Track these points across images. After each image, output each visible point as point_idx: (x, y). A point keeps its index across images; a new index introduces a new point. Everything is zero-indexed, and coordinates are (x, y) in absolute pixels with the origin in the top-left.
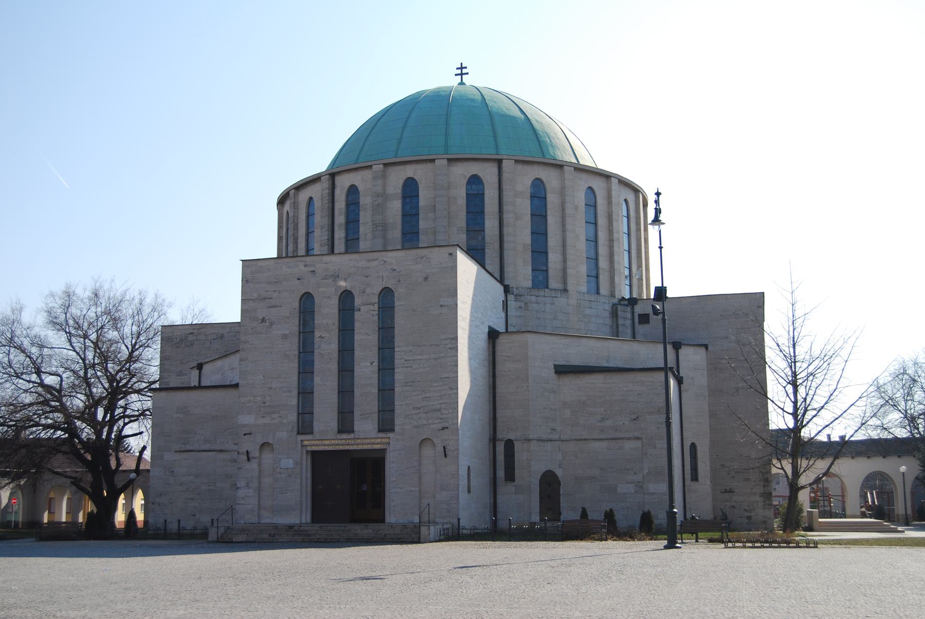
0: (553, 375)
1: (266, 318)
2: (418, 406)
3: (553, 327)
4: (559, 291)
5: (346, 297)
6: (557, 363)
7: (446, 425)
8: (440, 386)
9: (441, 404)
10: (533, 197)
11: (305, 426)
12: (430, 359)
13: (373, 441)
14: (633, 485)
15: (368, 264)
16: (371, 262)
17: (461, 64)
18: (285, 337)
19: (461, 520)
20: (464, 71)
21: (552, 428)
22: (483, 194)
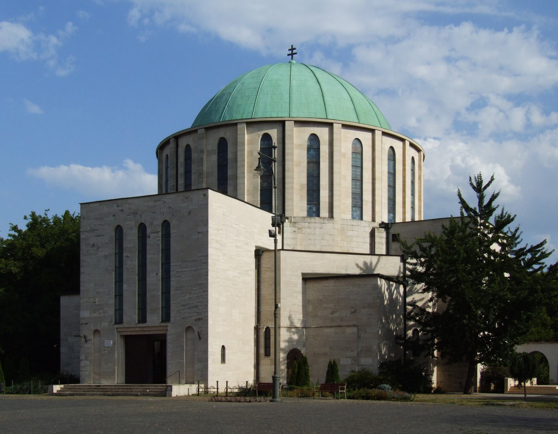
1: (95, 244)
3: (322, 245)
5: (142, 228)
6: (304, 272)
7: (200, 317)
9: (197, 302)
10: (309, 149)
11: (119, 320)
14: (351, 359)
17: (292, 46)
18: (106, 257)
19: (219, 383)
20: (294, 51)
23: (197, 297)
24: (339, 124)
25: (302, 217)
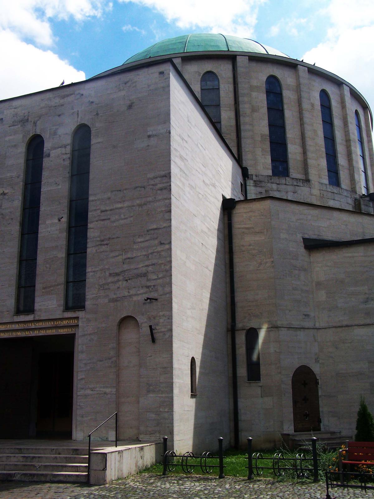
0: (302, 250)
2: (117, 271)
4: (301, 181)
6: (306, 236)
8: (147, 241)
9: (146, 266)
10: (268, 92)
12: (134, 206)
13: (59, 323)
15: (62, 101)
16: (66, 99)
21: (305, 313)
22: (219, 89)
23: (145, 255)
24: (305, 68)
25: (268, 176)
